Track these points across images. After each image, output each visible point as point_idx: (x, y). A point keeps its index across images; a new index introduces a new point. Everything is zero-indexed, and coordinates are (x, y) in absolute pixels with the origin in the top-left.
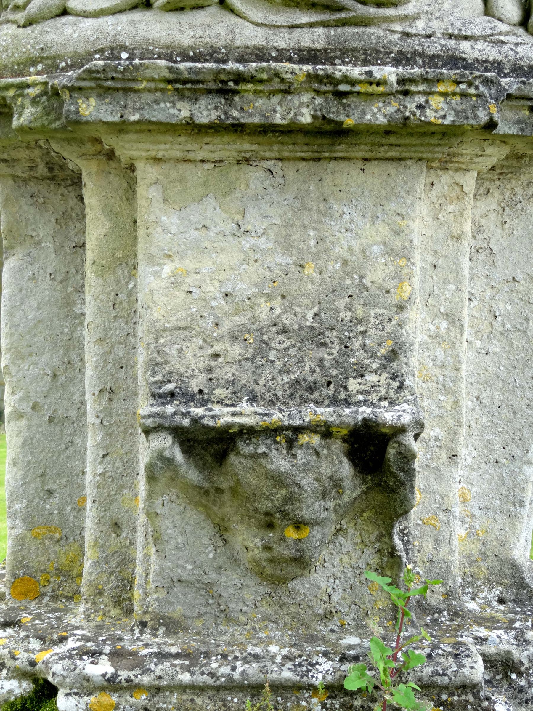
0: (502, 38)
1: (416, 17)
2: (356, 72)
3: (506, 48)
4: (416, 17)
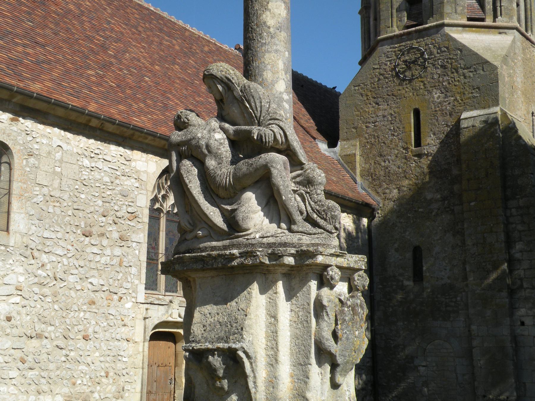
0: (278, 235)
1: (251, 234)
2: (228, 252)
3: (278, 238)
4: (251, 234)
